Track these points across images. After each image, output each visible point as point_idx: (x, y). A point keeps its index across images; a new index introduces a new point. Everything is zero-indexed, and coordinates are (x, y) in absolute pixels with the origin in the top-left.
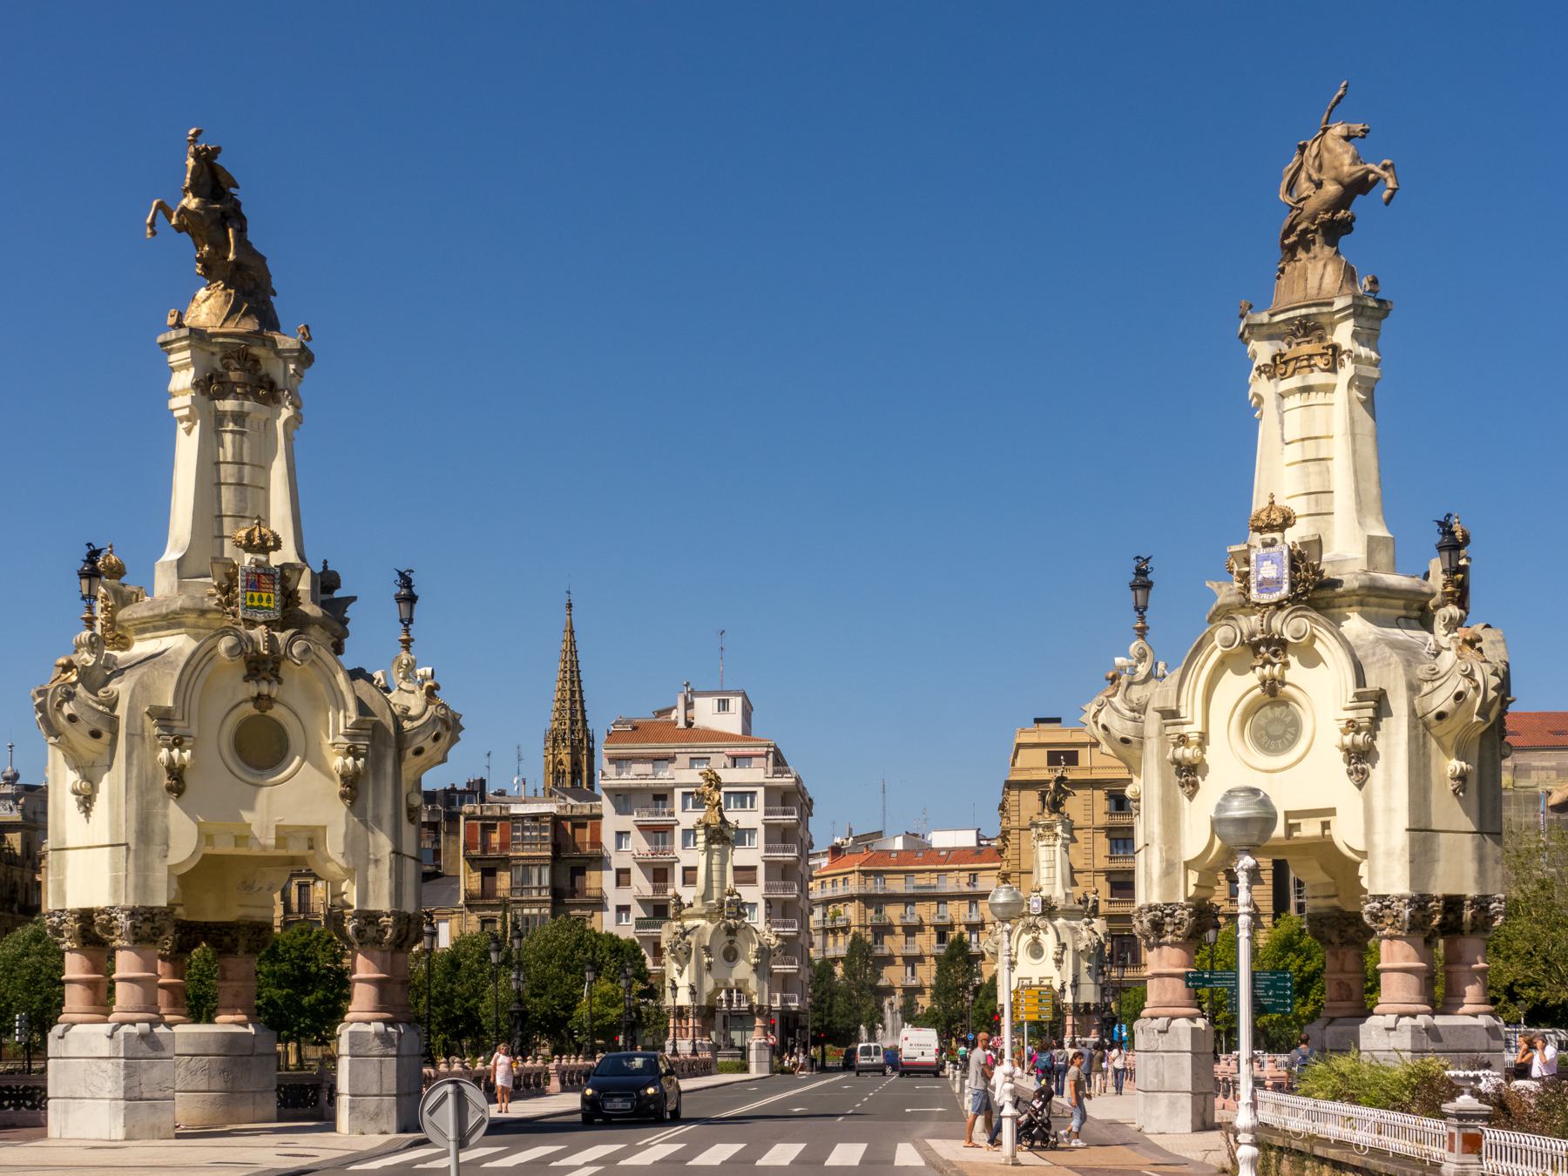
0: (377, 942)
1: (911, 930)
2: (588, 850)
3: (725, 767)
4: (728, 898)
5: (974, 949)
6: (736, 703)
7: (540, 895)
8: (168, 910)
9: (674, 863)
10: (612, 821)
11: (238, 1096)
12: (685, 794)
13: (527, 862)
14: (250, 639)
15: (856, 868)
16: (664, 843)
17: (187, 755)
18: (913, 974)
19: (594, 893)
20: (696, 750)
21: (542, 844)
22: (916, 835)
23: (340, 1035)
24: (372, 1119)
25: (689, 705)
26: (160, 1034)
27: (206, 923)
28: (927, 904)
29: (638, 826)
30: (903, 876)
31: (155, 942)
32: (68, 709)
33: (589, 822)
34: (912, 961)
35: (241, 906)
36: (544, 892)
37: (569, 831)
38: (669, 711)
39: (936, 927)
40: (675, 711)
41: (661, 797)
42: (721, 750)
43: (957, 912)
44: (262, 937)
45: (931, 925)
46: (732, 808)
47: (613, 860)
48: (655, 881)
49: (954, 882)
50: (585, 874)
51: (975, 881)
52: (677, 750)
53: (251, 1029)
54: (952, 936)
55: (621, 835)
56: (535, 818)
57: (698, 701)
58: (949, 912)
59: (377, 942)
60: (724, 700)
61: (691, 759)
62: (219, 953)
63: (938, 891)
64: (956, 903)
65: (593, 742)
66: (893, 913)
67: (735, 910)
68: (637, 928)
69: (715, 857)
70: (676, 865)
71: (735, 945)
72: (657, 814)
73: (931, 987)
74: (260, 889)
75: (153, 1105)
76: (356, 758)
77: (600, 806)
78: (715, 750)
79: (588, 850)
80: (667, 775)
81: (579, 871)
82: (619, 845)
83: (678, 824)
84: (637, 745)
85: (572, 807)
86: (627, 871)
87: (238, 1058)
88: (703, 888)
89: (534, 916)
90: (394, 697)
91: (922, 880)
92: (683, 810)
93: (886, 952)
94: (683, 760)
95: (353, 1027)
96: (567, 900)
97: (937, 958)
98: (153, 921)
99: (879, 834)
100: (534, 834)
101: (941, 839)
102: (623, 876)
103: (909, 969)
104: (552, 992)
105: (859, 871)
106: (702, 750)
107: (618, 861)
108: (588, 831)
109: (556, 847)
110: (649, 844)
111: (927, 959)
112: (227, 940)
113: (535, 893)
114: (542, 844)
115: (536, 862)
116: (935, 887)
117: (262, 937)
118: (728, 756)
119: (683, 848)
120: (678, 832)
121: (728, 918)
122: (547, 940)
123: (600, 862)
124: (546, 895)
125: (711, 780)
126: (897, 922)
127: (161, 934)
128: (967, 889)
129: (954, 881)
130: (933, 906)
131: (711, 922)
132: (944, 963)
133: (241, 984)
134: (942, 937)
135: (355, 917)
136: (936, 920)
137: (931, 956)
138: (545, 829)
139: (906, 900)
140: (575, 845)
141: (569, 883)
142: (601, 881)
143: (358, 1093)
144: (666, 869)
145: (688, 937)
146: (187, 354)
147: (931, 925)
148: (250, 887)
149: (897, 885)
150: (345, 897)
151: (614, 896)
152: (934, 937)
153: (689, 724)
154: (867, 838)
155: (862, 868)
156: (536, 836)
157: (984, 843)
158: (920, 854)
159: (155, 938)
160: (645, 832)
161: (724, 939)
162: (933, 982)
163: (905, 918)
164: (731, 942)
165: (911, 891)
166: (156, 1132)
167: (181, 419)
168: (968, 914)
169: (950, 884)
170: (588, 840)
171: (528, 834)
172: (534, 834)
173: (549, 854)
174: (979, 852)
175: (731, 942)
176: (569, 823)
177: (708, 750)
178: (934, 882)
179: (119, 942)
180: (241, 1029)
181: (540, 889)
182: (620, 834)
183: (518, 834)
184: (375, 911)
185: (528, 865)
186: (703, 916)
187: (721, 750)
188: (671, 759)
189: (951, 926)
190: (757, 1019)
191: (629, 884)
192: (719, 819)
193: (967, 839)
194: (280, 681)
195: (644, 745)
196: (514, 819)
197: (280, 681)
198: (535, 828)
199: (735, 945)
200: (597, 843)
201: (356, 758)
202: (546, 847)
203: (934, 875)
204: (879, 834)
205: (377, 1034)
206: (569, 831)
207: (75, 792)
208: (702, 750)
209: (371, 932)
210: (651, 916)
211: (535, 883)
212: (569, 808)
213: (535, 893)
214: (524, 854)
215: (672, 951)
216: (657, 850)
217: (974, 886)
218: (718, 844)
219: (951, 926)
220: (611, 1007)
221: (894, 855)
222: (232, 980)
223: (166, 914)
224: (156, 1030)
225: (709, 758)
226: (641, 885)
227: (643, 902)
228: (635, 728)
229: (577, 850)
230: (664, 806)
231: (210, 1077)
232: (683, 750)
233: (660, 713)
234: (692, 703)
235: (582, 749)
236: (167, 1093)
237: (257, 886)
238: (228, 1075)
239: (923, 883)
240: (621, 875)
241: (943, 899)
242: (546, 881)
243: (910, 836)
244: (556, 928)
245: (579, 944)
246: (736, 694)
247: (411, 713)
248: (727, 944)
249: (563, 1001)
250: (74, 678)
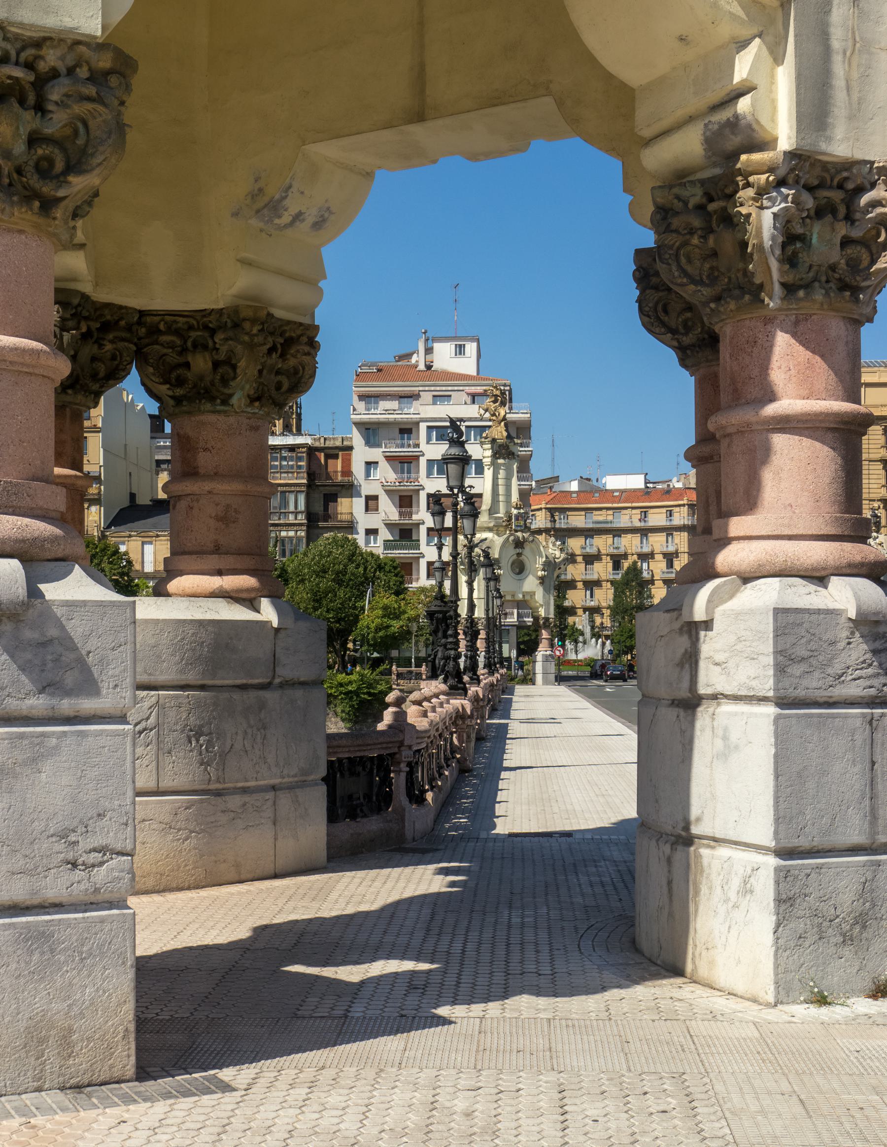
1: (590, 559)
2: (340, 478)
3: (466, 403)
5: (646, 575)
6: (471, 348)
7: (296, 519)
8: (104, 62)
9: (419, 490)
10: (361, 453)
11: (235, 801)
12: (429, 427)
13: (284, 489)
15: (543, 506)
16: (409, 472)
18: (592, 596)
19: (345, 517)
20: (438, 388)
21: (298, 473)
22: (589, 480)
23: (708, 625)
24: (847, 939)
25: (429, 351)
26: (71, 605)
27: (142, 313)
28: (604, 537)
29: (385, 457)
30: (583, 513)
31: (47, 205)
33: (340, 453)
34: (591, 585)
35: (247, 263)
36: (300, 517)
37: (323, 461)
38: (410, 355)
39: (612, 556)
40: (415, 356)
41: (407, 430)
42: (461, 388)
43: (630, 544)
44: (292, 362)
45: (607, 555)
46: (472, 441)
47: (363, 487)
48: (401, 506)
49: (628, 519)
50: (336, 501)
51: (671, 516)
52: (421, 388)
53: (268, 613)
54: (626, 565)
55: (370, 465)
56: (292, 448)
57: (437, 346)
58: (623, 543)
60: (460, 345)
61: (434, 396)
62: (178, 401)
63: (614, 525)
64: (629, 536)
65: (301, 408)
66: (575, 544)
67: (522, 523)
68: (385, 549)
69: (501, 471)
70: (421, 492)
72: (402, 446)
73: (609, 607)
74: (298, 217)
75: (43, 936)
77: (351, 438)
78: (456, 388)
79: (340, 478)
80: (412, 411)
81: (331, 498)
82: (368, 474)
83: (423, 455)
84: (384, 384)
85: (325, 439)
86: (375, 498)
87: (237, 696)
88: (490, 502)
89: (291, 538)
91: (599, 516)
92: (428, 443)
93: (569, 577)
94: (427, 397)
96: (321, 524)
97: (612, 583)
98: (40, 108)
99: (556, 479)
100: (290, 463)
101: (614, 482)
102: (371, 502)
103: (588, 592)
104: (327, 605)
105: (546, 508)
106: (444, 388)
107: (367, 489)
108: (340, 461)
109: (311, 476)
110: (395, 472)
111: (604, 584)
112: (201, 363)
113: (291, 517)
114: (298, 473)
115: (293, 489)
116: (611, 522)
117: (292, 362)
118: (468, 394)
119: (428, 477)
120: (423, 462)
121: (516, 531)
122: (321, 556)
123: (350, 489)
124: (302, 518)
125: (496, 396)
126: (578, 552)
127: (74, 167)
128: (638, 524)
129: (628, 517)
130: (609, 539)
131: (499, 535)
132: (620, 587)
133: (237, 486)
134: (617, 566)
135: (781, 183)
136: (612, 551)
137: (608, 581)
138: (300, 459)
139: (586, 533)
140: (327, 474)
141: (322, 508)
142: (352, 507)
143: (803, 842)
144: (411, 496)
147: (607, 555)
148: (275, 207)
149: (578, 521)
150: (744, 105)
151: (364, 521)
152: (610, 565)
153: (429, 367)
154: (545, 482)
155: (548, 506)
156: (292, 466)
157: (651, 485)
158: (597, 495)
159: (47, 189)
160: (392, 462)
161: (512, 552)
162: (611, 603)
163: (585, 548)
164: (519, 555)
165: (591, 526)
166: (51, 1054)
168: (639, 545)
169: (624, 520)
170: (339, 469)
171: (285, 463)
172: (290, 463)
173: (305, 481)
174: (648, 493)
175: (519, 555)
176: (323, 454)
177: (450, 388)
178: (610, 518)
180: (239, 613)
181: (296, 513)
182: (368, 464)
183: (276, 463)
184: (850, 165)
185: (285, 492)
186: (490, 529)
187: (461, 388)
188: (415, 396)
189: (625, 556)
190: (543, 631)
191: (377, 510)
192: (505, 434)
193: (636, 482)
195: (391, 383)
196: (272, 449)
198: (291, 459)
199: (523, 557)
200: (347, 471)
202: (302, 475)
203: (611, 512)
204: (556, 479)
206: (323, 461)
208: (444, 388)
210: (398, 538)
211: (292, 508)
212: (322, 440)
213: (291, 517)
214: (282, 482)
216: (403, 478)
217: (645, 521)
218: (504, 458)
219: (625, 556)
220: (393, 619)
221: (574, 495)
222: (216, 475)
223: (97, 77)
224: (52, 591)
225: (450, 396)
226: (388, 510)
227: (389, 526)
228: (379, 370)
229: (328, 477)
230: (409, 439)
231: (162, 750)
232: (427, 388)
233: (401, 358)
234: (432, 348)
235: (292, 413)
236: (101, 874)
237: (293, 206)
238: (210, 744)
239: (601, 518)
240: (370, 502)
241: (617, 532)
242: (302, 506)
243: (584, 480)
244: (329, 544)
245: (351, 558)
246: (472, 339)
248: (515, 557)
249: (338, 613)
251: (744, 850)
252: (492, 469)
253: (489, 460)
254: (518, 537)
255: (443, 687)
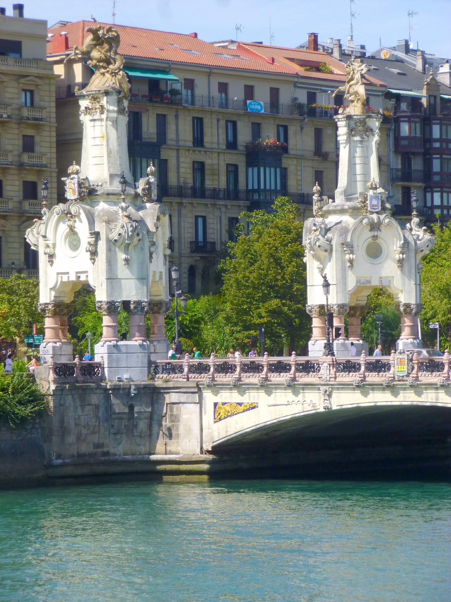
0: (410, 313)
4: (371, 192)
14: (372, 218)
17: (354, 256)
32: (318, 244)
59: (410, 313)
71: (379, 241)
76: (403, 255)
90: (413, 232)
95: (403, 341)
121: (372, 213)
145: (329, 235)
146: (345, 122)
164: (375, 237)
167: (342, 144)
175: (375, 237)
179: (313, 316)
190: (406, 319)
194: (380, 231)
197: (380, 231)
199: (379, 241)
201: (403, 255)
205: (411, 343)
207: (319, 268)
209: (408, 310)
215: (312, 249)
247: (420, 238)
248: (370, 240)
250: (318, 234)
251: (205, 409)
252: (348, 147)
253: (345, 137)
254: (373, 219)
255: (116, 109)
